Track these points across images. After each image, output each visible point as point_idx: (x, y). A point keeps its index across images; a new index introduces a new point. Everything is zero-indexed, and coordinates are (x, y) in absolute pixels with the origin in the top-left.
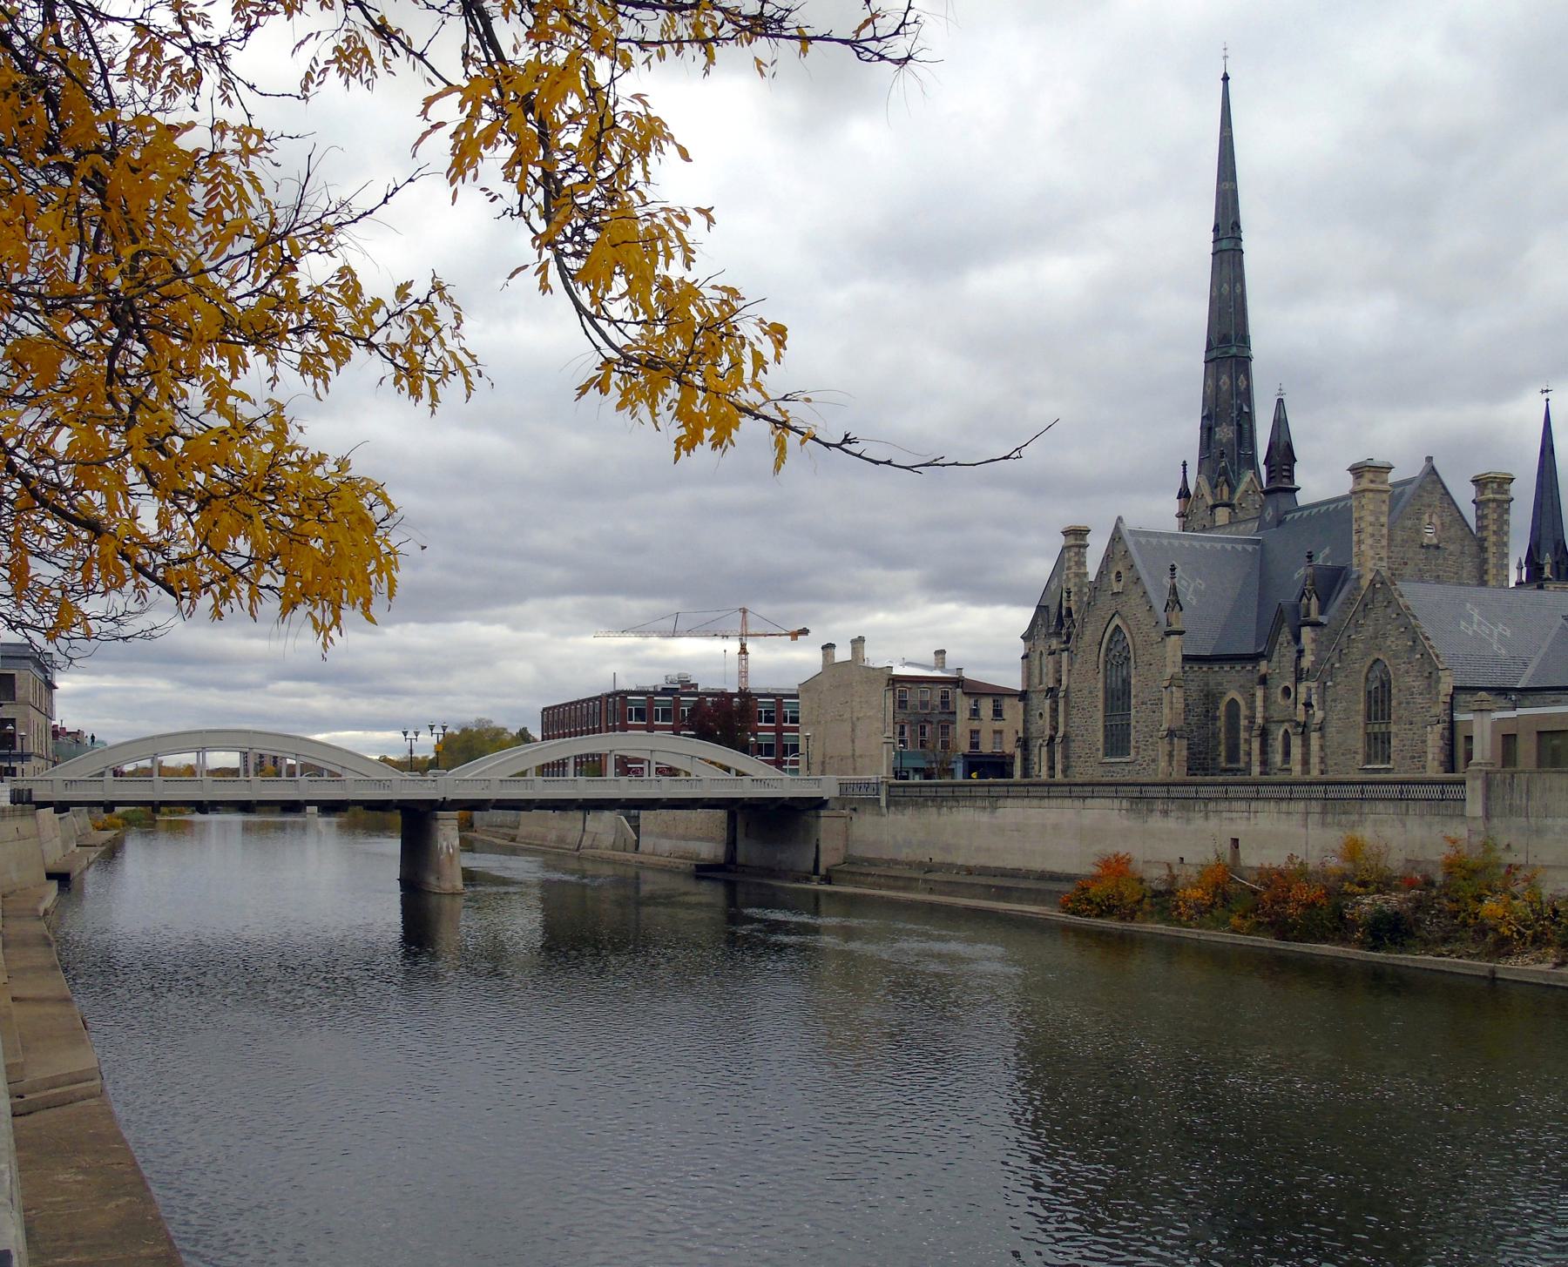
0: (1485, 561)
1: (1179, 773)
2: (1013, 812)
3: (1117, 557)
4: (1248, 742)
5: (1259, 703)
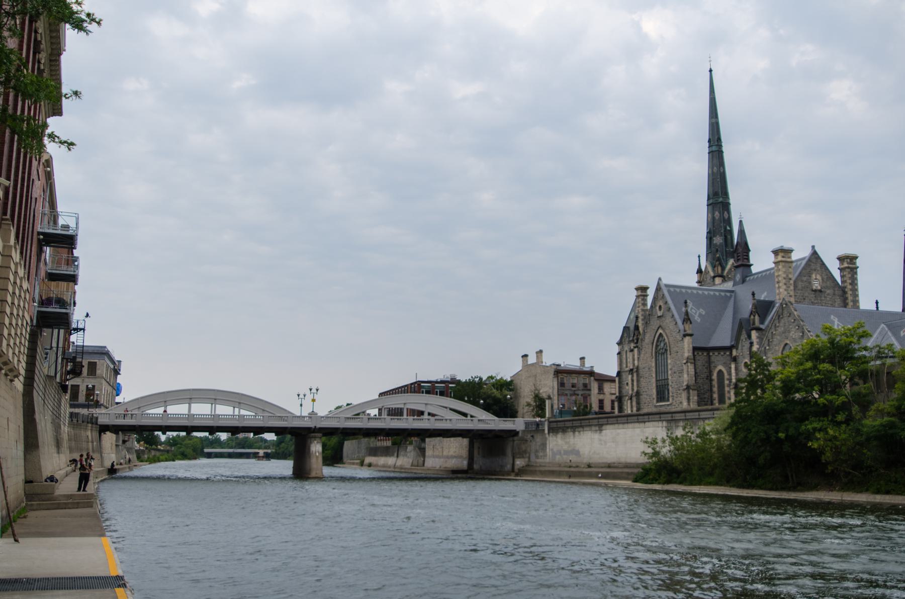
0: (846, 298)
1: (694, 406)
2: (611, 432)
3: (660, 297)
4: (729, 392)
5: (733, 371)
